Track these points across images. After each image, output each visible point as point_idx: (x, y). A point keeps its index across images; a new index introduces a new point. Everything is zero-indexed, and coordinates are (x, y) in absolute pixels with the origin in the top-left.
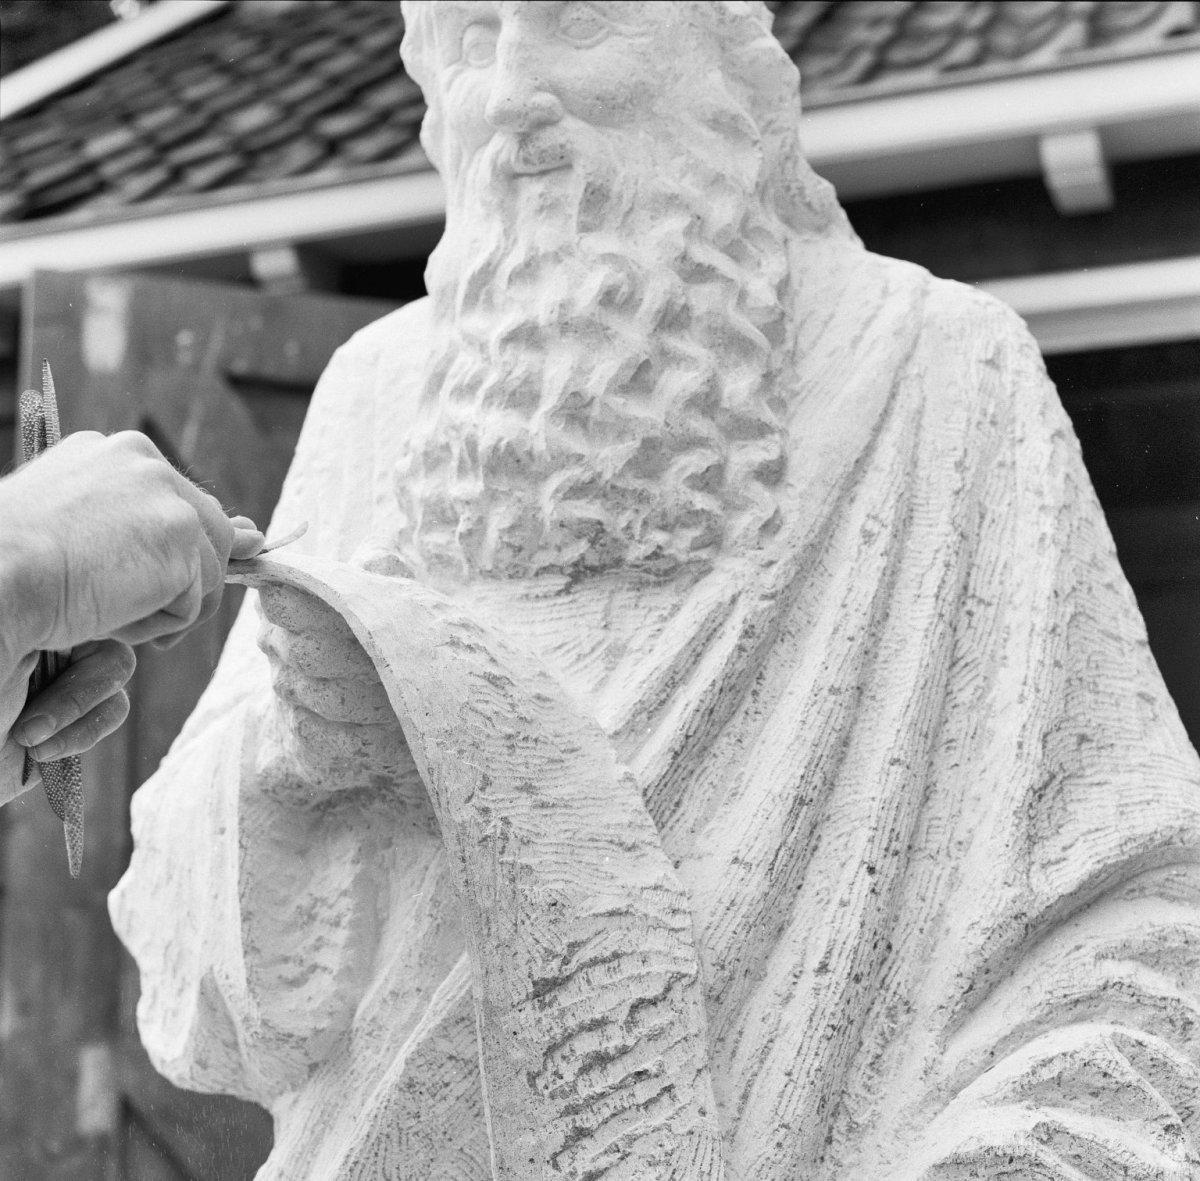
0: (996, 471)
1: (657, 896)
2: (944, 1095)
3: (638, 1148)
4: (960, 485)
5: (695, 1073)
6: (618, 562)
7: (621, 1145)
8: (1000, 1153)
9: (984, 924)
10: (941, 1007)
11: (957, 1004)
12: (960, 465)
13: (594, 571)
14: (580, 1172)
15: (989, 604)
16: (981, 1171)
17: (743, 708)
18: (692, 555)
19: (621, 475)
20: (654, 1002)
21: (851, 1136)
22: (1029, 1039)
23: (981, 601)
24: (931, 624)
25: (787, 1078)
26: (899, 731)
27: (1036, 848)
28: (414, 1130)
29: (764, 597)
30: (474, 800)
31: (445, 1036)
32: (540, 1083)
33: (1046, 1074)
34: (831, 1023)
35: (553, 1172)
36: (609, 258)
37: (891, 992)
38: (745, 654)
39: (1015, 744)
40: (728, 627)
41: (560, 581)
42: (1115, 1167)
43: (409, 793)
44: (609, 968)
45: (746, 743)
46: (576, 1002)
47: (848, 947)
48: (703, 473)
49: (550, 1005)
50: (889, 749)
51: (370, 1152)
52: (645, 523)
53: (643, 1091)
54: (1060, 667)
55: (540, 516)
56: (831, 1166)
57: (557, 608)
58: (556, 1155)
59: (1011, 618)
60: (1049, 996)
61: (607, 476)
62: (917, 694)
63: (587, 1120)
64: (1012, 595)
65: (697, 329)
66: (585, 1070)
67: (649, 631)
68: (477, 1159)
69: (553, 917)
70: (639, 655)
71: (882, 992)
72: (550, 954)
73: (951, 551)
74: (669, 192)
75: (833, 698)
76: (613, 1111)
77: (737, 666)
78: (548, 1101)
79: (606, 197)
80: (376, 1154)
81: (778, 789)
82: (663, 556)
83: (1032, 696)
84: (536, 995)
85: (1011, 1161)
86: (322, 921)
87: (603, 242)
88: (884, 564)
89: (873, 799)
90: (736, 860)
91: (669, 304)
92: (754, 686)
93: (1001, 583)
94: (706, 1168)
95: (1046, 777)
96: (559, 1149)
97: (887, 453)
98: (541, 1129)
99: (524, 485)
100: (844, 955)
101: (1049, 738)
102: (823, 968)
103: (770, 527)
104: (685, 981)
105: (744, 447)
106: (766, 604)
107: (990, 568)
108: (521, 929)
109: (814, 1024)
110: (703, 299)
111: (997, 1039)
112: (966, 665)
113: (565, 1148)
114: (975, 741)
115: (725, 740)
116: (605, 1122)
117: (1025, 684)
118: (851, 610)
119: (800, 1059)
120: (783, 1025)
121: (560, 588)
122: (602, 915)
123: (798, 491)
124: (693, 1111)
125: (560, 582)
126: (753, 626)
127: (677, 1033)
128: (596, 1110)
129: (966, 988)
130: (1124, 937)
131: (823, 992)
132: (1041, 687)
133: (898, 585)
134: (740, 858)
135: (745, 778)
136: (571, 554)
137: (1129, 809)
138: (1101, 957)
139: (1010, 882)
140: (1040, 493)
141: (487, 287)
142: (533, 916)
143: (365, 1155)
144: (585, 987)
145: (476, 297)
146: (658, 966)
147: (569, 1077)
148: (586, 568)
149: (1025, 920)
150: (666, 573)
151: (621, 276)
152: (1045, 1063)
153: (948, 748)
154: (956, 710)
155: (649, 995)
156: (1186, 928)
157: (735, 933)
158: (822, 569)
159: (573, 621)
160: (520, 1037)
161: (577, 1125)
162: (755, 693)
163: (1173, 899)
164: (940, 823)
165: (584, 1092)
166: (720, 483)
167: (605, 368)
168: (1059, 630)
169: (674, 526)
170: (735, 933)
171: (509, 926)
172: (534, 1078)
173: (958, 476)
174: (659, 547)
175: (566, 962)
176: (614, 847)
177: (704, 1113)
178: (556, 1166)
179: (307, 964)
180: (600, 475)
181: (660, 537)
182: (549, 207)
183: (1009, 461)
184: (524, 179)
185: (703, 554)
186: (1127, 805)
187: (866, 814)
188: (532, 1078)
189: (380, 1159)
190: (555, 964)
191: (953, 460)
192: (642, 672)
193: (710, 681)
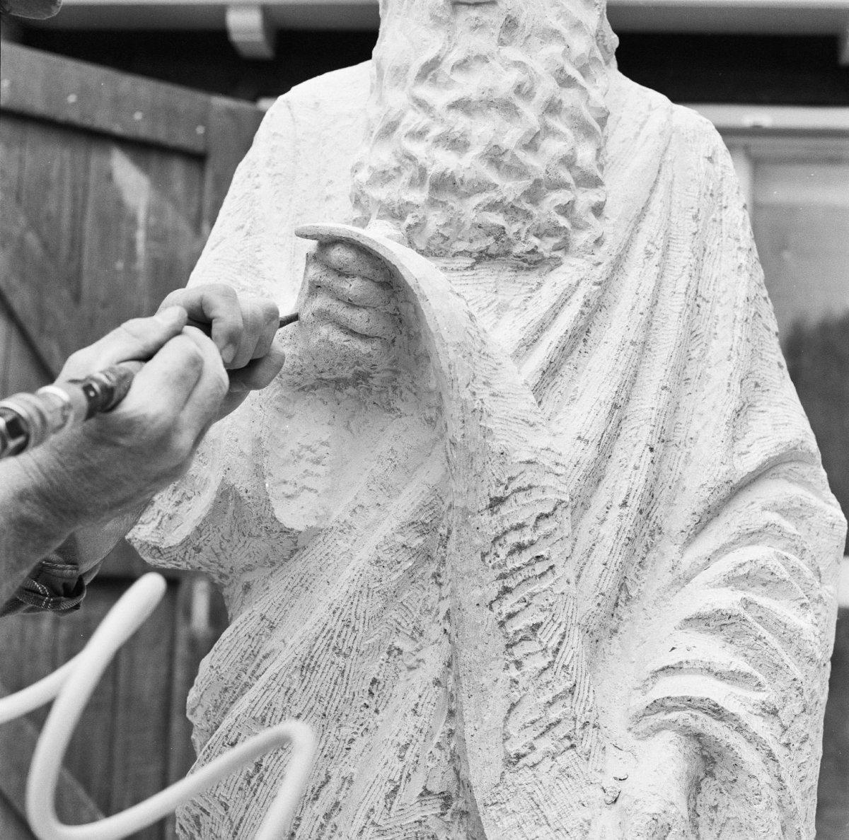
0: (711, 224)
1: (548, 454)
2: (682, 581)
3: (535, 600)
4: (696, 230)
5: (565, 559)
6: (507, 253)
7: (527, 598)
8: (724, 613)
9: (709, 485)
10: (682, 531)
11: (692, 529)
12: (695, 218)
13: (491, 256)
14: (504, 613)
15: (708, 302)
16: (712, 623)
17: (578, 349)
18: (553, 253)
19: (518, 200)
20: (547, 516)
21: (628, 603)
22: (728, 552)
23: (704, 299)
24: (683, 309)
25: (603, 567)
26: (666, 370)
27: (735, 444)
28: (377, 589)
29: (595, 284)
30: (470, 387)
31: (401, 533)
32: (487, 559)
33: (741, 572)
34: (628, 536)
35: (489, 612)
36: (518, 64)
37: (652, 521)
38: (583, 316)
39: (726, 385)
40: (573, 299)
41: (469, 261)
42: (780, 624)
43: (377, 383)
44: (526, 495)
45: (580, 369)
46: (514, 512)
47: (639, 493)
48: (566, 205)
49: (496, 512)
50: (661, 380)
51: (347, 602)
52: (528, 231)
53: (540, 568)
54: (749, 342)
55: (463, 219)
56: (616, 620)
57: (464, 278)
58: (492, 602)
59: (719, 311)
60: (739, 529)
61: (510, 199)
62: (676, 350)
63: (510, 583)
64: (720, 298)
65: (564, 116)
66: (511, 553)
67: (523, 297)
68: (410, 609)
69: (501, 461)
70: (518, 311)
71: (647, 521)
72: (499, 483)
73: (692, 268)
74: (554, 28)
75: (632, 347)
76: (523, 578)
77: (579, 323)
78: (490, 570)
79: (516, 26)
80: (352, 603)
81: (603, 399)
82: (537, 253)
83: (736, 358)
84: (491, 506)
85: (730, 617)
86: (307, 460)
87: (512, 53)
88: (658, 272)
89: (653, 408)
90: (579, 438)
91: (553, 98)
92: (585, 337)
93: (714, 290)
94: (570, 614)
95: (742, 404)
96: (494, 599)
97: (656, 206)
98: (485, 587)
99: (454, 198)
100: (636, 498)
101: (743, 382)
102: (624, 504)
103: (598, 242)
104: (563, 505)
105: (586, 191)
106: (596, 288)
107: (708, 281)
108: (487, 466)
109: (619, 536)
110: (569, 97)
111: (712, 551)
112: (696, 335)
113: (498, 598)
114: (700, 381)
115: (568, 367)
116: (519, 585)
117: (731, 350)
118: (641, 296)
119: (612, 555)
120: (601, 536)
121: (468, 265)
122: (523, 462)
123: (612, 222)
124: (564, 580)
125: (469, 261)
126: (589, 300)
127: (558, 534)
128: (515, 577)
129: (697, 522)
130: (774, 499)
131: (624, 518)
132: (740, 352)
133: (664, 284)
134: (582, 436)
135: (580, 390)
136: (477, 246)
137: (777, 427)
138: (764, 509)
139: (724, 462)
140: (737, 240)
141: (434, 72)
142: (492, 460)
143: (344, 603)
144: (514, 504)
145: (425, 77)
146: (552, 496)
147: (503, 557)
148: (487, 255)
149: (731, 484)
150: (535, 263)
151: (526, 76)
152: (741, 566)
153: (686, 383)
154: (690, 362)
155: (547, 511)
156: (802, 497)
157: (579, 480)
158: (622, 271)
159: (475, 286)
160: (480, 531)
161: (505, 585)
162: (585, 340)
163: (791, 481)
164: (681, 426)
165: (510, 566)
166: (571, 212)
167: (511, 137)
168: (748, 321)
169: (542, 235)
170: (579, 480)
171: (481, 464)
172: (484, 556)
173: (694, 224)
174: (536, 247)
175: (506, 488)
176: (524, 423)
177: (569, 583)
178: (491, 608)
179: (299, 486)
180: (505, 198)
181: (536, 241)
182: (477, 27)
183: (718, 219)
184: (463, 7)
185: (559, 254)
186: (777, 425)
187: (649, 417)
188: (484, 555)
189: (354, 606)
190: (502, 488)
191: (691, 214)
192: (521, 323)
193: (564, 331)
